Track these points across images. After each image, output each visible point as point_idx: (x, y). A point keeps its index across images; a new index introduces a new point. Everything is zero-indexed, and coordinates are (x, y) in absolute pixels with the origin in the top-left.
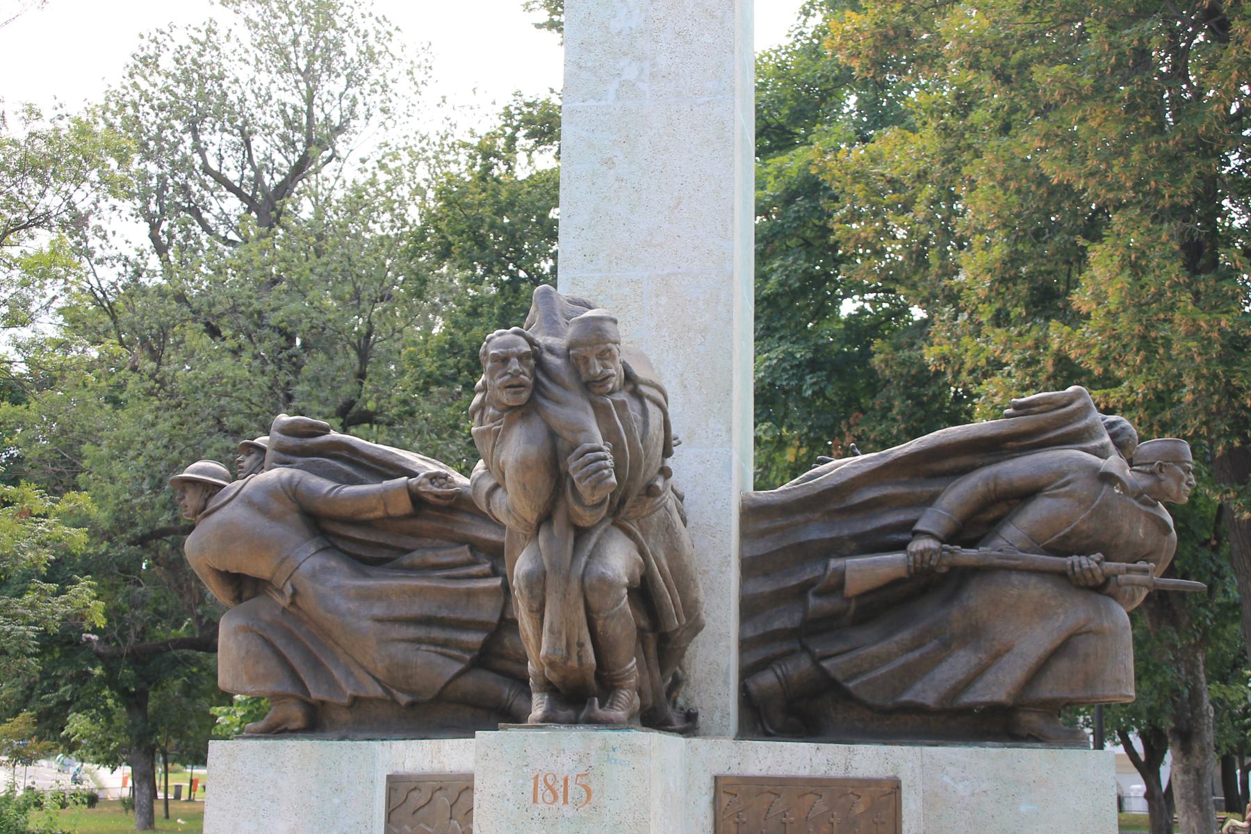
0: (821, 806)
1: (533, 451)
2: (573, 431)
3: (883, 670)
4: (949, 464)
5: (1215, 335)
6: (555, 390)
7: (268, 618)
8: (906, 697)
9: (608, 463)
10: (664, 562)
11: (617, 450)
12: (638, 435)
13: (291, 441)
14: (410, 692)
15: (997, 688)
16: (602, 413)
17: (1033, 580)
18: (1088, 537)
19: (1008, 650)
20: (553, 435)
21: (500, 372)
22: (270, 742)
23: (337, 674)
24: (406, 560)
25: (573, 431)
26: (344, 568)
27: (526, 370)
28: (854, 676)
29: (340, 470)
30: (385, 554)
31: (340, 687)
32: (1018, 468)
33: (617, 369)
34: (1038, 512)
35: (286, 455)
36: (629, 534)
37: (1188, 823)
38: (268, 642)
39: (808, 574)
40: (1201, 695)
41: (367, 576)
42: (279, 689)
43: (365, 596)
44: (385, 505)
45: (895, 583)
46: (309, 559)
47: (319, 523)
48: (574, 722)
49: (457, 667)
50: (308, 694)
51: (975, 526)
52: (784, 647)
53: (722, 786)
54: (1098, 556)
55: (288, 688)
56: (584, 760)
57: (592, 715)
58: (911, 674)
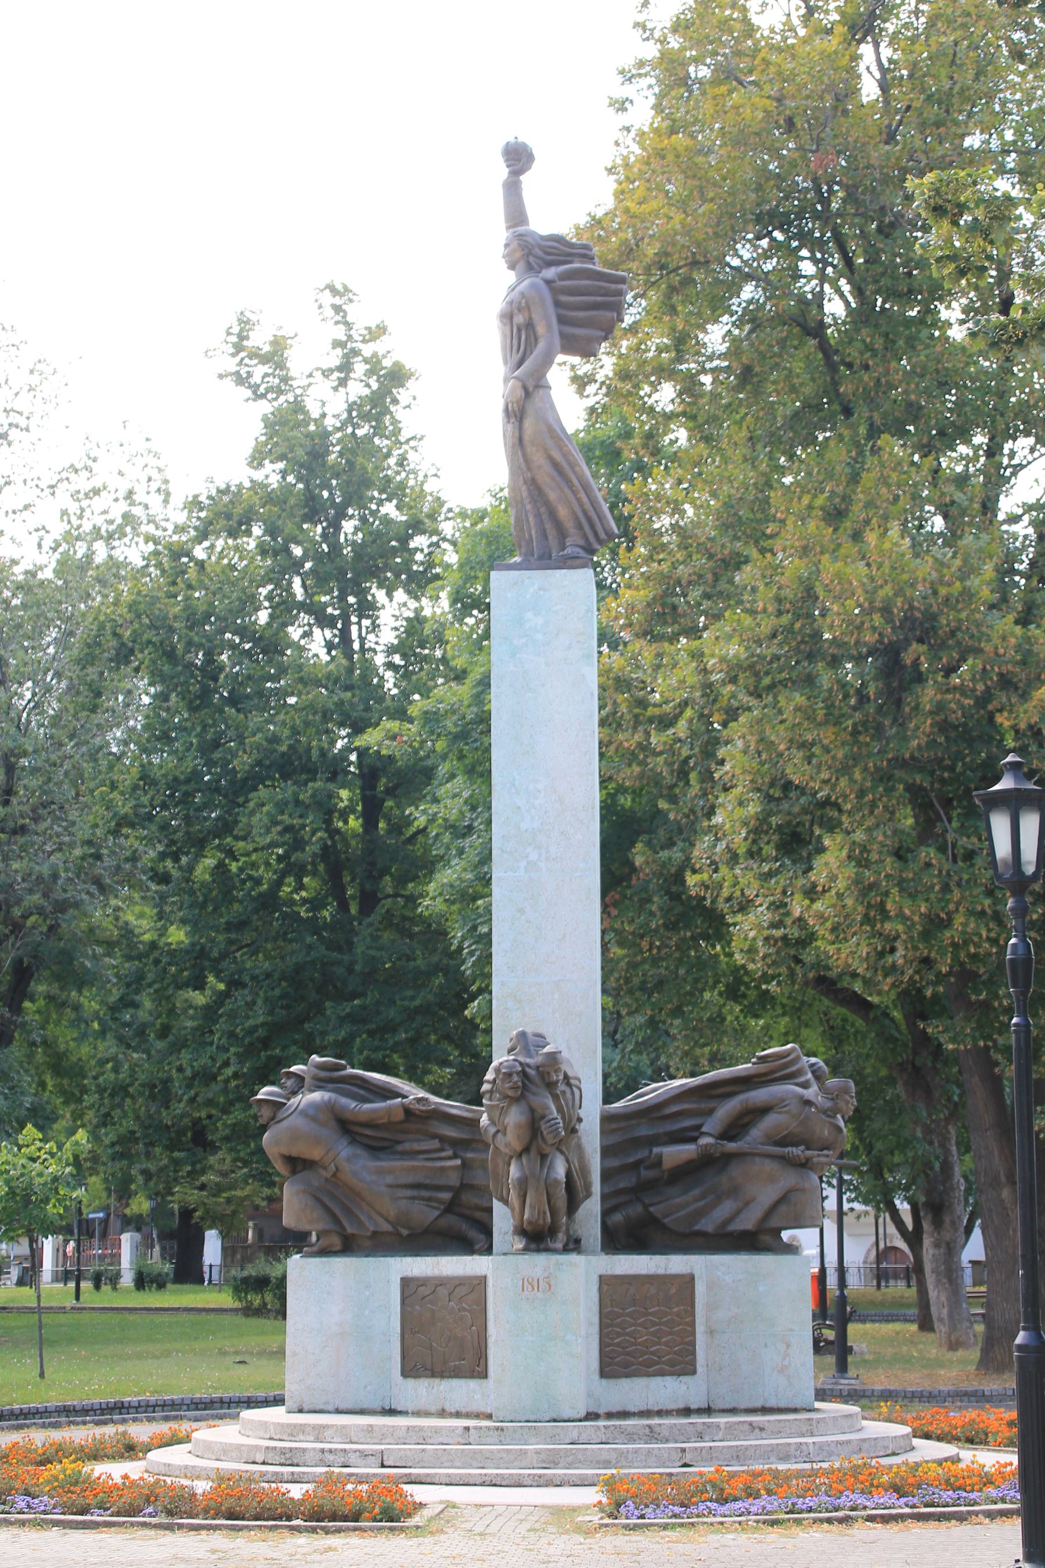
0: (653, 1290)
3: (683, 1212)
4: (721, 1090)
5: (916, 918)
6: (533, 1088)
7: (316, 1184)
8: (697, 1228)
11: (563, 1118)
13: (323, 1074)
14: (408, 1228)
15: (747, 1222)
16: (556, 1098)
17: (767, 1161)
20: (532, 1111)
22: (324, 1259)
23: (362, 1218)
24: (400, 1148)
28: (666, 1216)
30: (386, 1144)
32: (760, 1095)
34: (770, 1121)
35: (320, 1084)
37: (938, 1297)
38: (318, 1199)
39: (639, 1156)
40: (952, 1168)
41: (378, 1159)
42: (328, 1227)
43: (381, 1172)
45: (690, 1162)
46: (344, 1150)
47: (346, 1126)
48: (538, 1251)
49: (437, 1213)
50: (344, 1229)
51: (734, 1129)
52: (622, 1199)
53: (605, 1281)
54: (802, 1148)
55: (331, 1226)
58: (700, 1214)
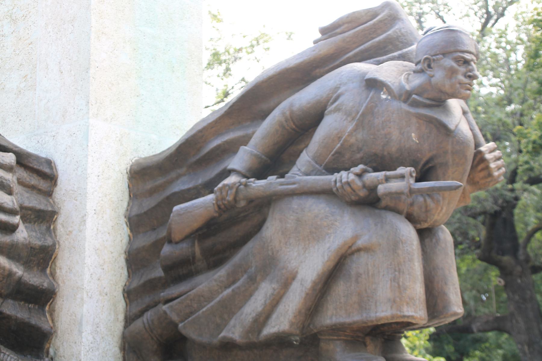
18: (359, 150)
19: (294, 278)
58: (229, 308)
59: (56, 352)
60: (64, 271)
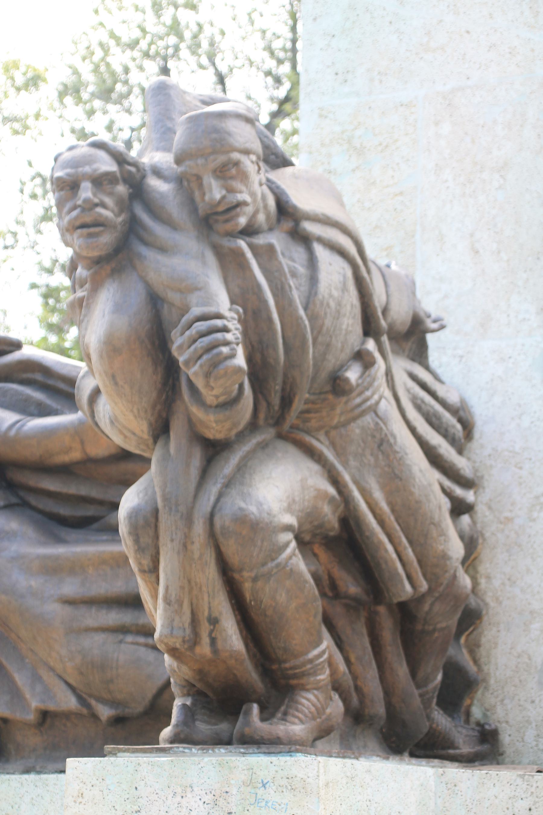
1: (123, 324)
2: (180, 291)
6: (159, 230)
9: (229, 336)
10: (378, 495)
12: (297, 297)
14: (112, 703)
16: (231, 264)
20: (155, 300)
21: (68, 206)
25: (180, 291)
26: (30, 531)
27: (108, 201)
29: (28, 400)
30: (90, 511)
31: (25, 699)
33: (253, 194)
36: (312, 453)
41: (60, 541)
43: (53, 569)
44: (82, 442)
56: (221, 802)
57: (247, 730)
59: (489, 713)
60: (496, 583)
